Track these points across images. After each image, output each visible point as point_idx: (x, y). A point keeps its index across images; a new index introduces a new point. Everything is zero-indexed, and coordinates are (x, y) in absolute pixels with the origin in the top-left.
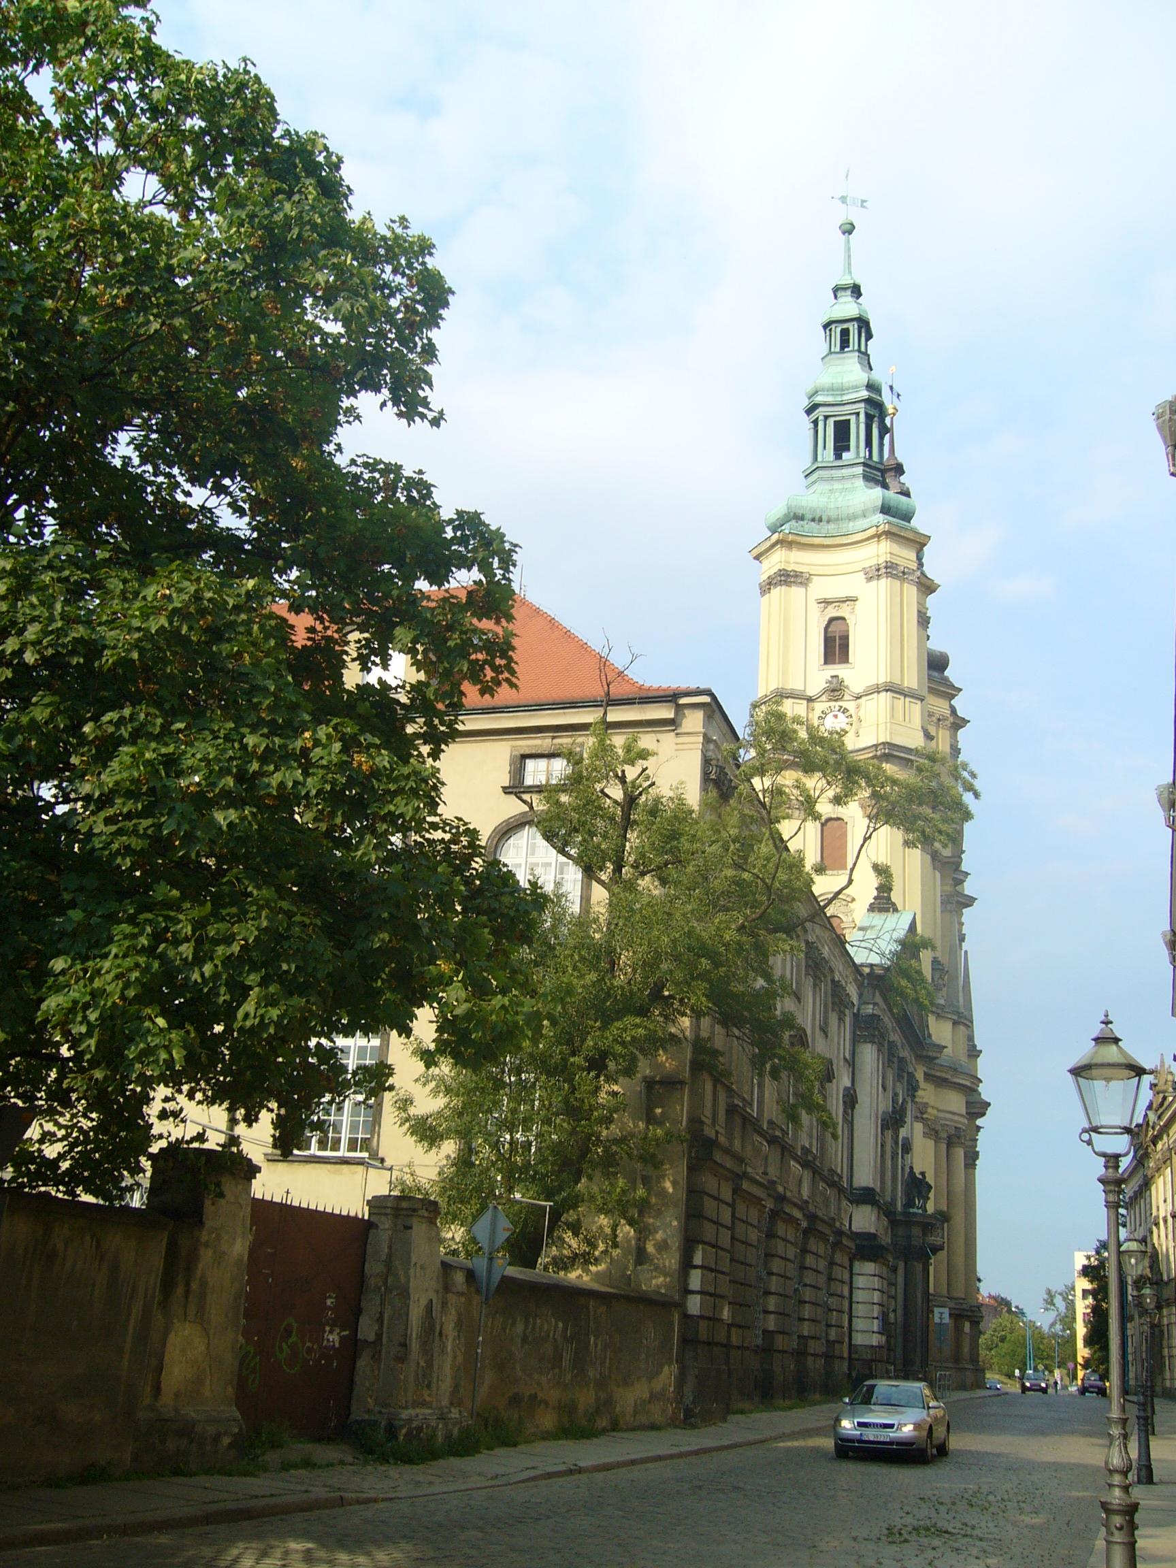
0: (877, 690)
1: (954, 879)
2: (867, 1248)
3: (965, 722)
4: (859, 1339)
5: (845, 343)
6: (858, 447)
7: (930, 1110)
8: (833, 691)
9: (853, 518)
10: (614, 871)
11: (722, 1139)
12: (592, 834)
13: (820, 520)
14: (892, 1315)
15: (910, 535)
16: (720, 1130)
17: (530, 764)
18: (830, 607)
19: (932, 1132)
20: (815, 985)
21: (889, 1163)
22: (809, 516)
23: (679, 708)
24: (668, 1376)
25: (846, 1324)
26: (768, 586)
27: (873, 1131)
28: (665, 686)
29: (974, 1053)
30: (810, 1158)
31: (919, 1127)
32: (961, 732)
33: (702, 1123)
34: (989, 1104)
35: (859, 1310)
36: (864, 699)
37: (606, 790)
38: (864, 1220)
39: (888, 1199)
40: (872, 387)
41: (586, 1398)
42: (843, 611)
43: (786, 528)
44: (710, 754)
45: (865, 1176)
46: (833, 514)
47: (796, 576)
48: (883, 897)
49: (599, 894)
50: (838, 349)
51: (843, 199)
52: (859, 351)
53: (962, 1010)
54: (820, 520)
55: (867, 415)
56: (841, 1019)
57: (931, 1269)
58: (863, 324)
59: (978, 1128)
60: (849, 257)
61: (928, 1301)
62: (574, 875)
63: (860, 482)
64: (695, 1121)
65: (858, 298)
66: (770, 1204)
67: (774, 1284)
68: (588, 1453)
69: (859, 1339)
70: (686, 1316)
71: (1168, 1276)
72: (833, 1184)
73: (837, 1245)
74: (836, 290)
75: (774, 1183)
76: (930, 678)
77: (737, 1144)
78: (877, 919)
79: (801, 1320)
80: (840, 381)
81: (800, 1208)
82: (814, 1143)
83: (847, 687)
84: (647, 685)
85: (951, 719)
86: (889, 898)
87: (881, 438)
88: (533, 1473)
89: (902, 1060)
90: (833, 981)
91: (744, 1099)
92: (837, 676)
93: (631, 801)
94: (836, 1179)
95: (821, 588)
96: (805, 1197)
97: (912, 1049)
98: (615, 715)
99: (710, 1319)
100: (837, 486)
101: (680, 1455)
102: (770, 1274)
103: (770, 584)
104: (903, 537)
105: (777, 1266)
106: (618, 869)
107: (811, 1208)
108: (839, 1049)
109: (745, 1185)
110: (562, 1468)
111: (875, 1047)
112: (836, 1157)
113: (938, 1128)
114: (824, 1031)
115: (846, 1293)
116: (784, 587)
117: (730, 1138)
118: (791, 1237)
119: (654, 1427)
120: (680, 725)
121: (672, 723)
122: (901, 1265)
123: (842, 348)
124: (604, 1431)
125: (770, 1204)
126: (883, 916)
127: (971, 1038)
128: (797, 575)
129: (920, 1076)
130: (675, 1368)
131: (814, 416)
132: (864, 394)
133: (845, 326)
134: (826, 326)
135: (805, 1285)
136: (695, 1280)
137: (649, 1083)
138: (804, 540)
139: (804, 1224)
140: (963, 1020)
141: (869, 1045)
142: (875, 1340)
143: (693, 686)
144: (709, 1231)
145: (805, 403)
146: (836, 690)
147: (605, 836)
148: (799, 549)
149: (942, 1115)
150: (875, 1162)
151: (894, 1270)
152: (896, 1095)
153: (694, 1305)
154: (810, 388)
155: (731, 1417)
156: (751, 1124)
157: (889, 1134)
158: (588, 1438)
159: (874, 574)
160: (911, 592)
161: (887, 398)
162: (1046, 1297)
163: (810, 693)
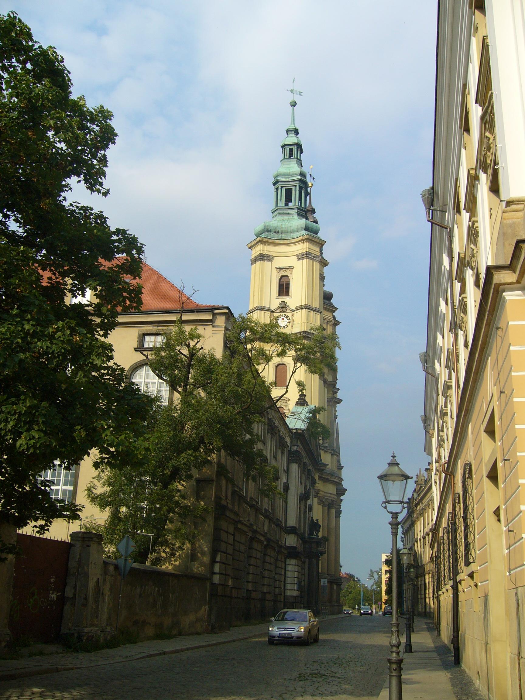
0: (301, 308)
1: (333, 391)
2: (292, 553)
4: (288, 593)
5: (291, 155)
6: (295, 201)
7: (320, 492)
8: (282, 308)
9: (292, 232)
13: (278, 232)
16: (229, 502)
17: (147, 338)
18: (282, 271)
19: (322, 502)
22: (273, 230)
23: (214, 315)
24: (204, 610)
26: (254, 261)
28: (208, 304)
29: (340, 467)
31: (316, 500)
33: (221, 498)
34: (346, 490)
35: (289, 580)
36: (296, 312)
37: (181, 351)
38: (291, 541)
40: (302, 174)
42: (287, 273)
43: (263, 235)
45: (292, 522)
46: (284, 230)
47: (267, 257)
49: (177, 396)
50: (288, 157)
51: (292, 91)
52: (297, 158)
53: (335, 449)
55: (300, 187)
56: (283, 453)
57: (320, 562)
58: (299, 146)
60: (294, 117)
62: (165, 390)
63: (296, 216)
64: (218, 498)
65: (297, 135)
66: (250, 534)
67: (252, 569)
69: (288, 593)
70: (212, 584)
71: (421, 564)
72: (277, 525)
74: (288, 131)
76: (324, 303)
78: (299, 409)
79: (263, 585)
80: (288, 171)
81: (264, 536)
82: (270, 507)
83: (288, 306)
84: (200, 304)
86: (304, 400)
90: (279, 436)
91: (240, 488)
93: (192, 355)
94: (279, 523)
95: (279, 262)
96: (266, 531)
98: (185, 317)
99: (223, 585)
100: (286, 217)
103: (255, 260)
105: (253, 561)
107: (268, 536)
108: (281, 466)
109: (240, 526)
111: (297, 465)
112: (280, 514)
114: (275, 458)
116: (261, 261)
119: (197, 634)
120: (215, 322)
122: (307, 560)
123: (290, 157)
125: (250, 534)
126: (302, 407)
127: (339, 461)
128: (268, 256)
129: (316, 477)
130: (207, 607)
131: (276, 186)
132: (299, 177)
133: (291, 147)
134: (283, 147)
135: (265, 570)
137: (198, 481)
138: (269, 240)
139: (265, 543)
140: (336, 453)
142: (295, 593)
144: (223, 546)
145: (273, 180)
146: (283, 307)
148: (269, 245)
149: (326, 494)
150: (297, 515)
151: (304, 562)
152: (306, 486)
153: (216, 579)
154: (275, 173)
155: (231, 628)
157: (303, 503)
159: (301, 257)
160: (317, 265)
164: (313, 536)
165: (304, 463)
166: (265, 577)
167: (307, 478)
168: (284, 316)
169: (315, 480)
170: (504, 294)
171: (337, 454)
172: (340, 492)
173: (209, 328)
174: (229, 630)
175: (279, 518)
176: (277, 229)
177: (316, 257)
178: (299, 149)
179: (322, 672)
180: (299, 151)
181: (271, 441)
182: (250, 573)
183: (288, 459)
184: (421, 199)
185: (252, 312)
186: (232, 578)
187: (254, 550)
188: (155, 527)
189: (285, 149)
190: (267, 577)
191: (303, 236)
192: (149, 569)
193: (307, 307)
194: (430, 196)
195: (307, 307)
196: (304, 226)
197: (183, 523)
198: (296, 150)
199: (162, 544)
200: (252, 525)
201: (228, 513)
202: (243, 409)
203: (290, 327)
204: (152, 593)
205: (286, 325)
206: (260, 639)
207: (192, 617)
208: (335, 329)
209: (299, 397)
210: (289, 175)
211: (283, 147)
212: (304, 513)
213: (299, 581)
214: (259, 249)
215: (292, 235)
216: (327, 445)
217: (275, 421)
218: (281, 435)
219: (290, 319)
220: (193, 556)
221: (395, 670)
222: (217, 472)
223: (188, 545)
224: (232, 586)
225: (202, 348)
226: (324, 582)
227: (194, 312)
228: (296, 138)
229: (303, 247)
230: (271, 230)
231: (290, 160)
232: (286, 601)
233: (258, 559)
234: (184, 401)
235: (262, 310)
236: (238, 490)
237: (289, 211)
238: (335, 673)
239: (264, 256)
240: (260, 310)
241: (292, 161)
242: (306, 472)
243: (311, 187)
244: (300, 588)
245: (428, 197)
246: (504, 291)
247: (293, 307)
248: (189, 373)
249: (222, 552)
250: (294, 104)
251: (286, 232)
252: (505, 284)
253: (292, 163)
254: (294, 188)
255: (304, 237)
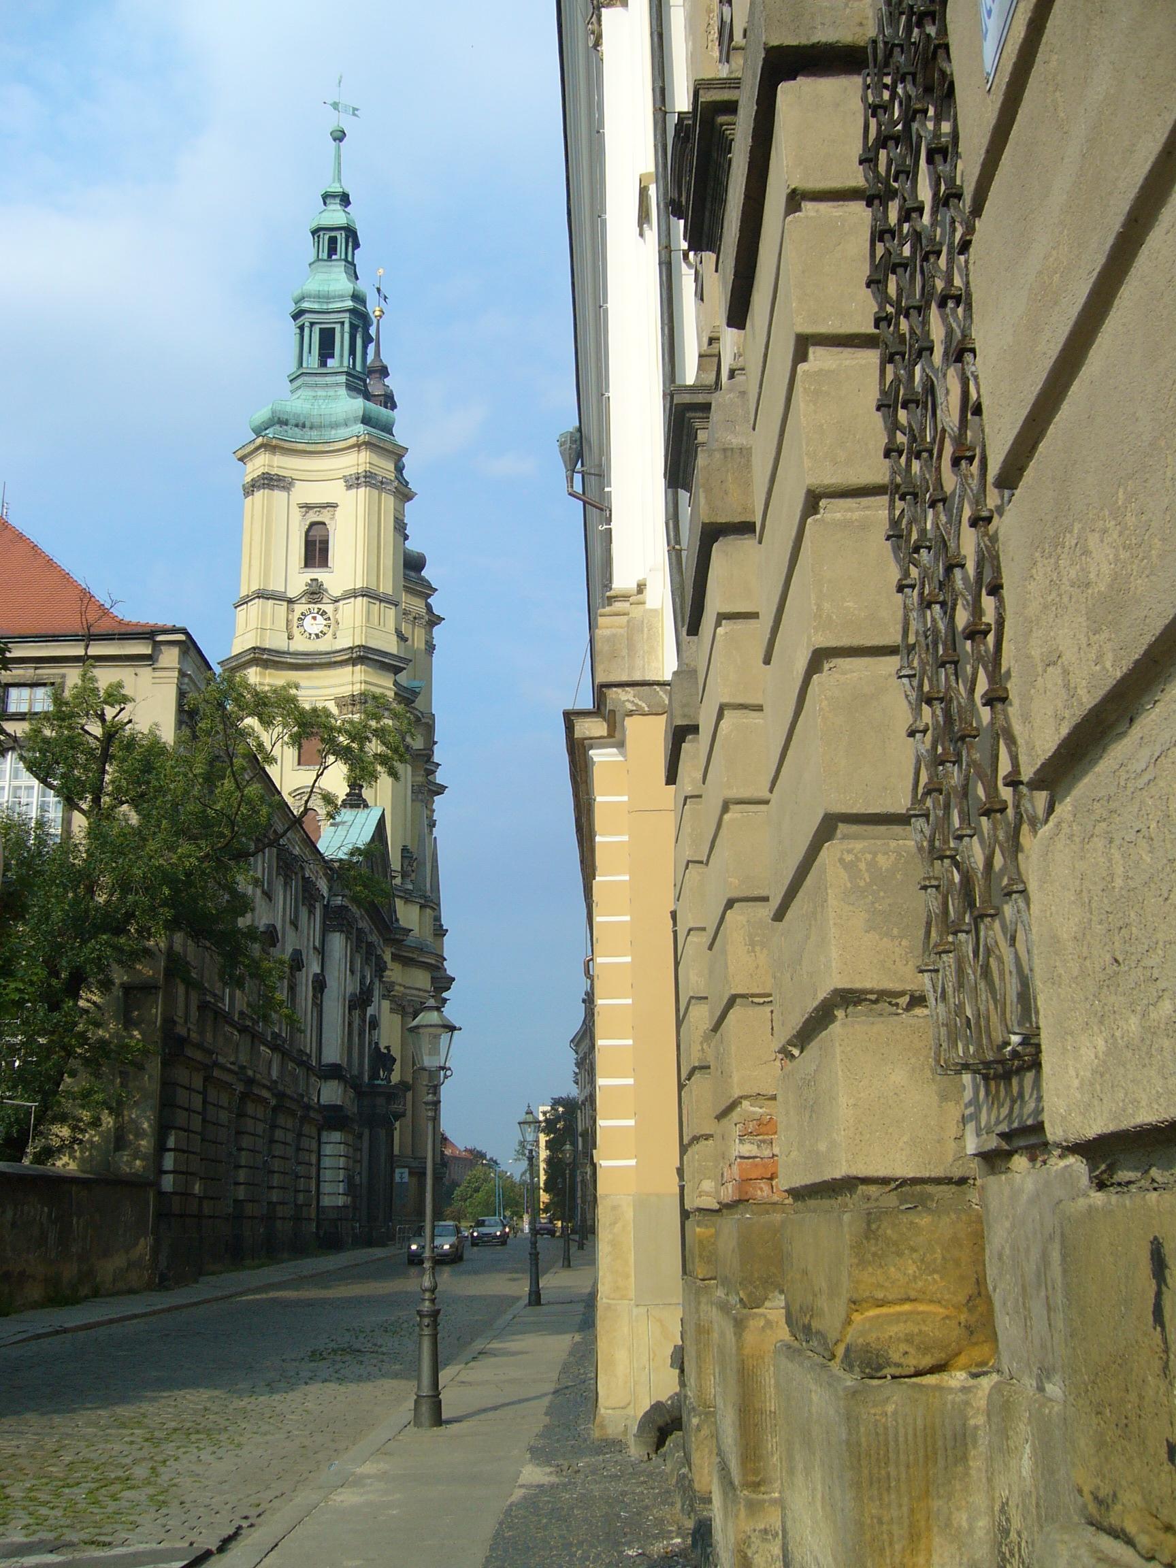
0: (353, 594)
1: (426, 770)
2: (334, 1118)
3: (440, 619)
4: (326, 1201)
5: (332, 250)
6: (342, 356)
7: (397, 988)
8: (313, 593)
9: (335, 426)
10: (93, 800)
11: (193, 1035)
12: (71, 768)
13: (304, 426)
14: (357, 1178)
15: (390, 447)
16: (192, 1027)
18: (311, 512)
20: (286, 884)
21: (356, 1039)
22: (293, 422)
23: (157, 645)
24: (144, 1246)
25: (314, 1189)
26: (251, 488)
27: (341, 1011)
28: (143, 622)
29: (440, 932)
30: (279, 1042)
31: (386, 1004)
32: (407, 505)
33: (175, 1023)
34: (453, 979)
35: (327, 1175)
36: (342, 602)
37: (86, 727)
38: (331, 1093)
39: (355, 1072)
40: (357, 297)
41: (69, 1271)
42: (324, 517)
43: (270, 432)
44: (184, 687)
45: (333, 1053)
46: (316, 420)
47: (280, 480)
48: (355, 794)
49: (80, 822)
50: (325, 257)
51: (335, 106)
52: (346, 260)
53: (429, 894)
54: (304, 426)
55: (351, 324)
56: (311, 912)
57: (396, 1134)
58: (351, 234)
59: (445, 1000)
60: (339, 164)
61: (392, 1163)
62: (55, 812)
63: (343, 391)
64: (169, 1021)
65: (346, 207)
66: (240, 1087)
67: (244, 1158)
68: (73, 1317)
69: (326, 1201)
70: (160, 1194)
72: (301, 1063)
73: (305, 1119)
74: (326, 197)
75: (245, 1067)
76: (406, 578)
77: (209, 1036)
79: (271, 1188)
80: (326, 289)
81: (268, 1088)
82: (284, 1027)
83: (326, 591)
84: (127, 619)
85: (427, 617)
86: (360, 795)
87: (365, 347)
88: (24, 1336)
89: (370, 945)
90: (303, 877)
91: (215, 995)
92: (317, 580)
93: (110, 735)
94: (305, 1058)
95: (304, 493)
96: (274, 1078)
97: (381, 934)
98: (96, 650)
99: (182, 1194)
100: (321, 393)
101: (154, 1313)
102: (240, 1149)
103: (253, 486)
104: (382, 448)
105: (246, 1142)
106: (96, 800)
107: (280, 1087)
108: (308, 940)
109: (216, 1073)
110: (50, 1329)
111: (343, 936)
112: (307, 1042)
113: (405, 1003)
114: (295, 924)
115: (314, 1160)
116: (266, 491)
117: (202, 1033)
118: (260, 1115)
119: (131, 1291)
120: (157, 660)
121: (149, 659)
122: (366, 1132)
123: (330, 256)
124: (86, 1298)
125: (240, 1087)
126: (354, 812)
127: (437, 919)
128: (280, 479)
129: (387, 957)
130: (150, 1239)
131: (300, 321)
132: (349, 304)
133: (333, 234)
134: (315, 232)
135: (274, 1157)
136: (169, 1162)
137: (127, 989)
138: (287, 445)
139: (273, 1102)
140: (430, 903)
141: (338, 934)
142: (341, 1201)
143: (170, 624)
144: (181, 1118)
145: (292, 308)
146: (315, 593)
147: (86, 769)
148: (283, 454)
149: (408, 991)
150: (343, 1039)
151: (360, 1136)
152: (363, 978)
153: (168, 1183)
154: (297, 293)
155: (201, 1279)
156: (221, 1017)
157: (357, 1013)
158: (72, 1304)
159: (353, 482)
160: (389, 501)
161: (373, 307)
162: (518, 1148)
163: (291, 594)
164: (379, 1082)
165: (360, 930)
166: (274, 1172)
167: (367, 961)
168: (316, 611)
169: (385, 962)
170: (591, 752)
171: (431, 905)
172: (441, 985)
173: (146, 673)
174: (197, 1282)
175: (305, 1047)
176: (302, 420)
177: (387, 483)
178: (350, 240)
179: (357, 1346)
180: (350, 244)
181: (285, 892)
182: (241, 1167)
183: (324, 923)
184: (558, 449)
185: (246, 603)
186: (201, 1178)
187: (180, 1091)
188: (41, 1091)
189: (319, 237)
190: (278, 1172)
191: (358, 437)
192: (31, 1172)
193: (367, 593)
194: (574, 446)
195: (367, 593)
196: (361, 414)
197: (97, 1075)
198: (344, 240)
199: (54, 1120)
200: (243, 1068)
201: (189, 1052)
202: (215, 847)
203: (329, 636)
204: (38, 1218)
205: (321, 632)
206: (258, 1297)
207: (118, 1261)
208: (431, 632)
209: (348, 790)
210: (328, 298)
211: (315, 232)
212: (360, 1034)
213: (349, 1175)
214: (261, 464)
215: (334, 433)
216: (410, 887)
217: (294, 847)
218: (307, 876)
219: (329, 619)
220: (119, 1140)
221: (428, 1326)
222: (167, 969)
223: (108, 1121)
224: (202, 1195)
225: (130, 721)
226: (402, 1175)
227: (114, 639)
228: (343, 214)
229: (358, 461)
230: (287, 420)
231: (330, 263)
232: (321, 1217)
233: (259, 1136)
234: (94, 833)
235: (268, 599)
236: (213, 1000)
237: (327, 379)
238: (380, 1346)
239: (272, 479)
240: (263, 597)
241: (336, 266)
242: (364, 950)
243: (381, 317)
244: (352, 1188)
245: (570, 448)
246: (591, 748)
247: (336, 592)
248: (104, 772)
249: (180, 1129)
250: (339, 136)
251: (321, 427)
252: (591, 738)
253: (337, 270)
254: (338, 327)
255: (361, 438)
